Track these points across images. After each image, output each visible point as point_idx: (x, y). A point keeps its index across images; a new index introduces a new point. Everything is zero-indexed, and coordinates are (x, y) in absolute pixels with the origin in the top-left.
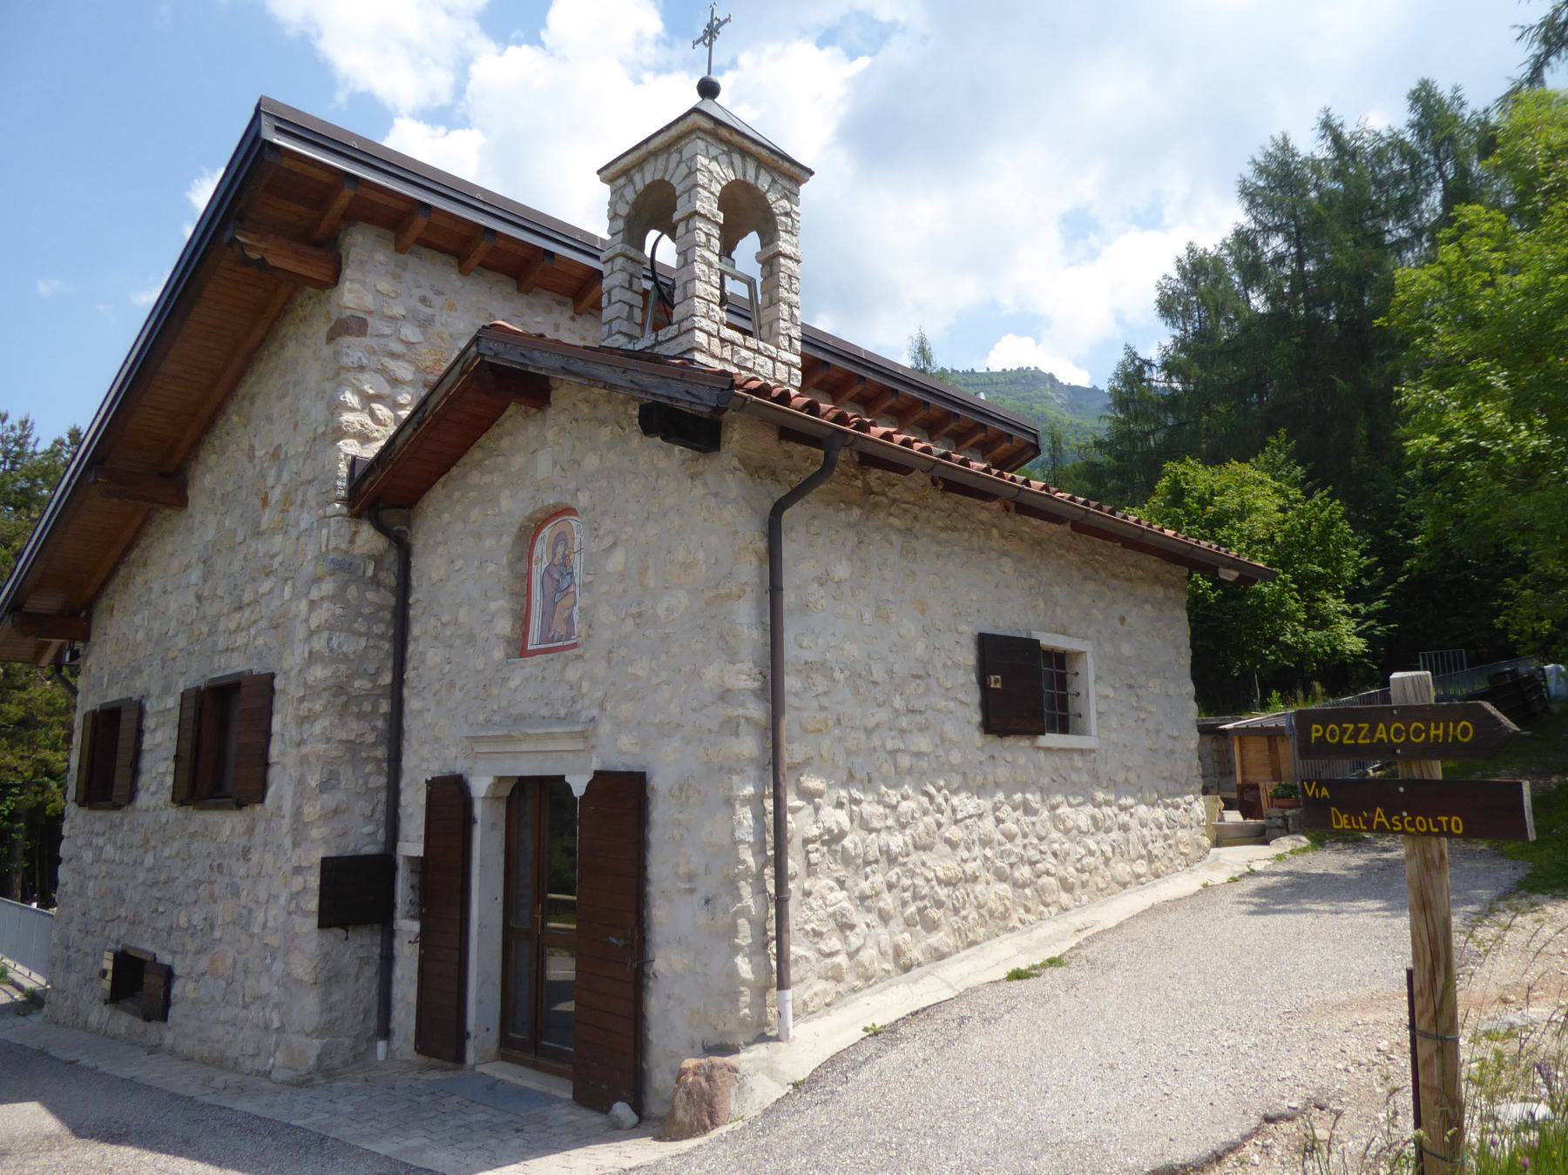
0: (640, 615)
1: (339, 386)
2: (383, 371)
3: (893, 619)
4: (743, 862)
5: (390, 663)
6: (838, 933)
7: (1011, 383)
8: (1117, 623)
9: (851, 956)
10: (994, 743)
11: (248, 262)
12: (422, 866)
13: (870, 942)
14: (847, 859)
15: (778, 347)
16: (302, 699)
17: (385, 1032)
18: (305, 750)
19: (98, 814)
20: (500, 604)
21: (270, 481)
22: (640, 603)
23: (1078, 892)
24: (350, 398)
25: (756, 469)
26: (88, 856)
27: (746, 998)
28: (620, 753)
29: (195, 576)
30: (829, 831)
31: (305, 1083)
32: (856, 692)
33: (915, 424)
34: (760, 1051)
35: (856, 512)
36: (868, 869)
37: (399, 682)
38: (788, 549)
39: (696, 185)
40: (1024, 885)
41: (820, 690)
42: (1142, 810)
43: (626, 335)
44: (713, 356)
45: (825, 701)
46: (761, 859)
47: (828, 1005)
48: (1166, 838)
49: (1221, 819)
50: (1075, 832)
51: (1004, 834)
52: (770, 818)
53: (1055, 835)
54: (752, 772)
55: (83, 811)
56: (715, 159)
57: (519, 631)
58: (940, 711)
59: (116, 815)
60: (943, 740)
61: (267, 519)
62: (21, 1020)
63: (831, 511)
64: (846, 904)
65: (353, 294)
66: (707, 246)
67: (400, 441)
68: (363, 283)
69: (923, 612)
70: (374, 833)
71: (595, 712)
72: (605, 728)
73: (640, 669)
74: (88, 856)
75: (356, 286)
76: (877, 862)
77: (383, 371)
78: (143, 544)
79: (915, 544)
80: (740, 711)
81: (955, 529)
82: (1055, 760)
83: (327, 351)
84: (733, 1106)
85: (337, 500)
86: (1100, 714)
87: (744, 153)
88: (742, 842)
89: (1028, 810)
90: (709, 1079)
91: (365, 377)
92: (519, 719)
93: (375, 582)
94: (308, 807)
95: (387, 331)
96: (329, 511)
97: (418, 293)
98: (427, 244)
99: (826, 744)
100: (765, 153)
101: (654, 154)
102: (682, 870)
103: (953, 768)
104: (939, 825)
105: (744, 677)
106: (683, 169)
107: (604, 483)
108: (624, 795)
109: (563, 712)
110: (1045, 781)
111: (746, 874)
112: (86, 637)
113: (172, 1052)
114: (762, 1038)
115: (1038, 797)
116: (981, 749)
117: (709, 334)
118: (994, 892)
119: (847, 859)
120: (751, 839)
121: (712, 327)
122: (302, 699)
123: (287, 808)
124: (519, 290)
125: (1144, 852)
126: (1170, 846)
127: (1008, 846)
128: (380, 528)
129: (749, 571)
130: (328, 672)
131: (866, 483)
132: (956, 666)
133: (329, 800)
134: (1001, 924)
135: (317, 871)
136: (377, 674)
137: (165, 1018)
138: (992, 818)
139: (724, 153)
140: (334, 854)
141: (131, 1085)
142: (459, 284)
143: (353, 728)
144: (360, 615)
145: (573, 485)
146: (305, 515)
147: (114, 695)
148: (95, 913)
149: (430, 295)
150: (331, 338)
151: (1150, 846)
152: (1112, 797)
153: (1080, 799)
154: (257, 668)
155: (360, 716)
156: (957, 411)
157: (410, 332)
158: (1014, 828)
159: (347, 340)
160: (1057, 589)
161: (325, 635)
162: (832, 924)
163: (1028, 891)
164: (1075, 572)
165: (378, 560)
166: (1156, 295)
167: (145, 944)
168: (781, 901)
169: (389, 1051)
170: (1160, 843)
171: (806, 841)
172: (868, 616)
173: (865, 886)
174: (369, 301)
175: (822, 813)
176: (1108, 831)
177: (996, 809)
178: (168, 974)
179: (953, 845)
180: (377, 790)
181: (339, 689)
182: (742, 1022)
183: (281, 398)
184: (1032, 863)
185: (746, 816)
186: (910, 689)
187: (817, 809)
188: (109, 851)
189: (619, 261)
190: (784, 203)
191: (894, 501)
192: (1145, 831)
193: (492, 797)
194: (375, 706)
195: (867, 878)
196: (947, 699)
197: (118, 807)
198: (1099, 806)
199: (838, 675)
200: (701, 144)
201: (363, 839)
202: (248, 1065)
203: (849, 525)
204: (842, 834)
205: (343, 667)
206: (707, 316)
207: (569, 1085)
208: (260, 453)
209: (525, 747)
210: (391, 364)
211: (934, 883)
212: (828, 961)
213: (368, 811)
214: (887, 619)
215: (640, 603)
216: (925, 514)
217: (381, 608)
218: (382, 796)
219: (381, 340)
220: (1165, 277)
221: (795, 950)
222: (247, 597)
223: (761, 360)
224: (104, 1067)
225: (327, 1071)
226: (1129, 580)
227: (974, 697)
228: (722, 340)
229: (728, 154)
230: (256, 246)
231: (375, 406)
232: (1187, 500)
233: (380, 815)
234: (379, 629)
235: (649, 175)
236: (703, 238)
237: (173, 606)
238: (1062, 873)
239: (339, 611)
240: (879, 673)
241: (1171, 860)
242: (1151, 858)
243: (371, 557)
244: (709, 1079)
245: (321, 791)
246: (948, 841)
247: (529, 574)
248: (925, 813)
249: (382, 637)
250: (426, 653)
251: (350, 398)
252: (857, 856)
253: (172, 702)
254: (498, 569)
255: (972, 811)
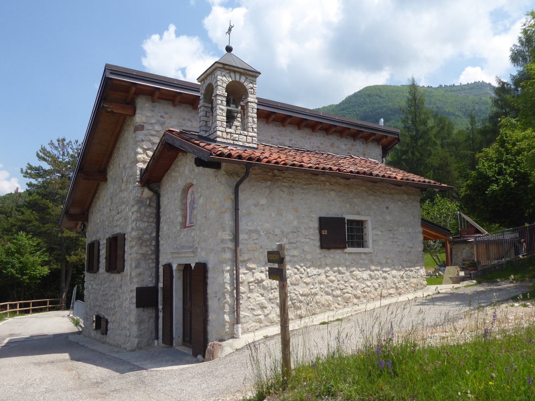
0: (206, 217)
1: (137, 148)
2: (149, 140)
3: (284, 214)
4: (226, 288)
5: (155, 230)
6: (261, 309)
7: (471, 89)
8: (385, 209)
9: (266, 316)
10: (326, 252)
11: (108, 112)
12: (164, 288)
13: (272, 312)
14: (264, 288)
15: (248, 132)
16: (131, 241)
17: (157, 338)
18: (132, 256)
19: (92, 274)
20: (179, 213)
21: (123, 175)
22: (206, 213)
23: (362, 299)
24: (140, 150)
25: (230, 174)
26: (90, 287)
27: (227, 326)
28: (201, 257)
29: (109, 203)
30: (258, 280)
31: (133, 350)
32: (269, 238)
33: (347, 135)
34: (231, 341)
35: (269, 183)
36: (272, 291)
37: (158, 236)
38: (242, 196)
39: (218, 85)
40: (338, 296)
41: (255, 238)
42: (394, 272)
43: (204, 131)
44: (224, 138)
45: (256, 241)
46: (232, 288)
47: (256, 330)
48: (405, 281)
49: (458, 275)
50: (361, 279)
51: (329, 280)
52: (235, 276)
53: (352, 280)
54: (229, 263)
55: (89, 274)
56: (224, 76)
57: (184, 221)
58: (303, 242)
59: (95, 275)
60: (304, 251)
61: (123, 186)
62: (78, 335)
63: (259, 183)
64: (263, 301)
65: (139, 118)
66: (222, 104)
67: (150, 165)
68: (142, 114)
69: (296, 212)
70: (152, 281)
71: (197, 245)
72: (199, 250)
73: (206, 233)
74: (90, 287)
75: (140, 115)
76: (276, 289)
77: (149, 140)
78: (98, 192)
79: (292, 190)
80: (226, 245)
81: (311, 184)
82: (354, 256)
83: (134, 135)
84: (219, 355)
85: (137, 182)
86: (374, 241)
87: (235, 72)
88: (226, 283)
89: (340, 272)
90: (213, 347)
91: (144, 143)
92: (183, 247)
93: (150, 206)
94: (135, 273)
95: (150, 128)
96: (135, 185)
97: (159, 115)
98: (162, 99)
99: (256, 254)
100: (242, 70)
101: (209, 75)
102: (214, 291)
103: (308, 260)
104: (301, 278)
105: (227, 235)
106: (215, 80)
107: (198, 177)
108: (202, 268)
109: (191, 245)
110: (348, 263)
111: (227, 292)
112: (87, 221)
113: (108, 344)
114: (233, 337)
115: (345, 268)
116: (320, 254)
117: (222, 132)
118: (324, 299)
119: (264, 288)
120: (229, 282)
121: (223, 129)
122: (131, 241)
123: (129, 274)
124: (193, 109)
125: (394, 286)
126: (407, 284)
127: (331, 284)
128: (150, 189)
129: (229, 204)
130: (136, 233)
131: (273, 173)
132: (310, 228)
133: (138, 271)
134: (327, 308)
135: (135, 291)
136: (151, 233)
137: (106, 334)
138: (324, 276)
139: (228, 73)
140: (140, 286)
141: (94, 350)
142: (173, 110)
143: (144, 250)
144: (145, 216)
145: (193, 177)
146: (131, 186)
147: (94, 239)
148: (92, 304)
149: (164, 115)
150: (134, 132)
151: (397, 284)
152: (379, 268)
153: (364, 269)
154: (122, 232)
155: (146, 246)
156: (363, 130)
157: (157, 128)
158: (334, 278)
159: (138, 132)
160: (356, 200)
161: (135, 222)
162: (258, 306)
163: (339, 298)
164: (365, 193)
165: (150, 199)
166: (510, 53)
167: (102, 314)
168: (238, 299)
169: (158, 343)
170: (403, 283)
171: (249, 283)
172: (273, 215)
173: (271, 296)
174: (144, 119)
175: (255, 274)
176: (377, 279)
177: (326, 272)
178: (107, 322)
179: (307, 284)
180: (153, 268)
181: (140, 238)
182: (226, 333)
183: (125, 149)
184: (341, 290)
185: (227, 276)
186: (291, 236)
187: (253, 273)
188: (94, 286)
189: (202, 108)
190: (251, 85)
191: (284, 178)
192: (395, 279)
193: (178, 270)
194: (151, 243)
195: (272, 293)
196: (306, 238)
197: (95, 273)
198: (373, 271)
199: (261, 233)
200: (219, 72)
201: (148, 282)
202: (123, 346)
203: (266, 187)
204: (262, 281)
205: (140, 232)
206: (222, 126)
207: (191, 350)
208: (121, 166)
209: (183, 255)
210: (152, 138)
211: (299, 295)
212: (257, 317)
213: (150, 274)
214: (282, 215)
215: (206, 213)
216: (297, 180)
217: (152, 213)
218: (154, 270)
219: (149, 131)
220: (514, 45)
221: (242, 313)
222: (120, 211)
223: (241, 137)
224: (89, 347)
225: (139, 347)
226: (391, 194)
227: (318, 237)
228: (227, 133)
229: (229, 73)
230: (109, 107)
231: (148, 152)
232: (506, 144)
233: (154, 275)
234: (151, 220)
235: (207, 82)
236: (220, 102)
237: (105, 212)
238: (355, 292)
239: (139, 215)
240: (277, 231)
241: (407, 289)
242: (397, 288)
243: (148, 198)
244: (213, 347)
245: (136, 268)
246: (305, 283)
247: (186, 203)
248: (296, 274)
249: (152, 222)
250: (164, 227)
251: (140, 150)
252: (268, 287)
253: (105, 242)
254: (178, 202)
255: (315, 273)
